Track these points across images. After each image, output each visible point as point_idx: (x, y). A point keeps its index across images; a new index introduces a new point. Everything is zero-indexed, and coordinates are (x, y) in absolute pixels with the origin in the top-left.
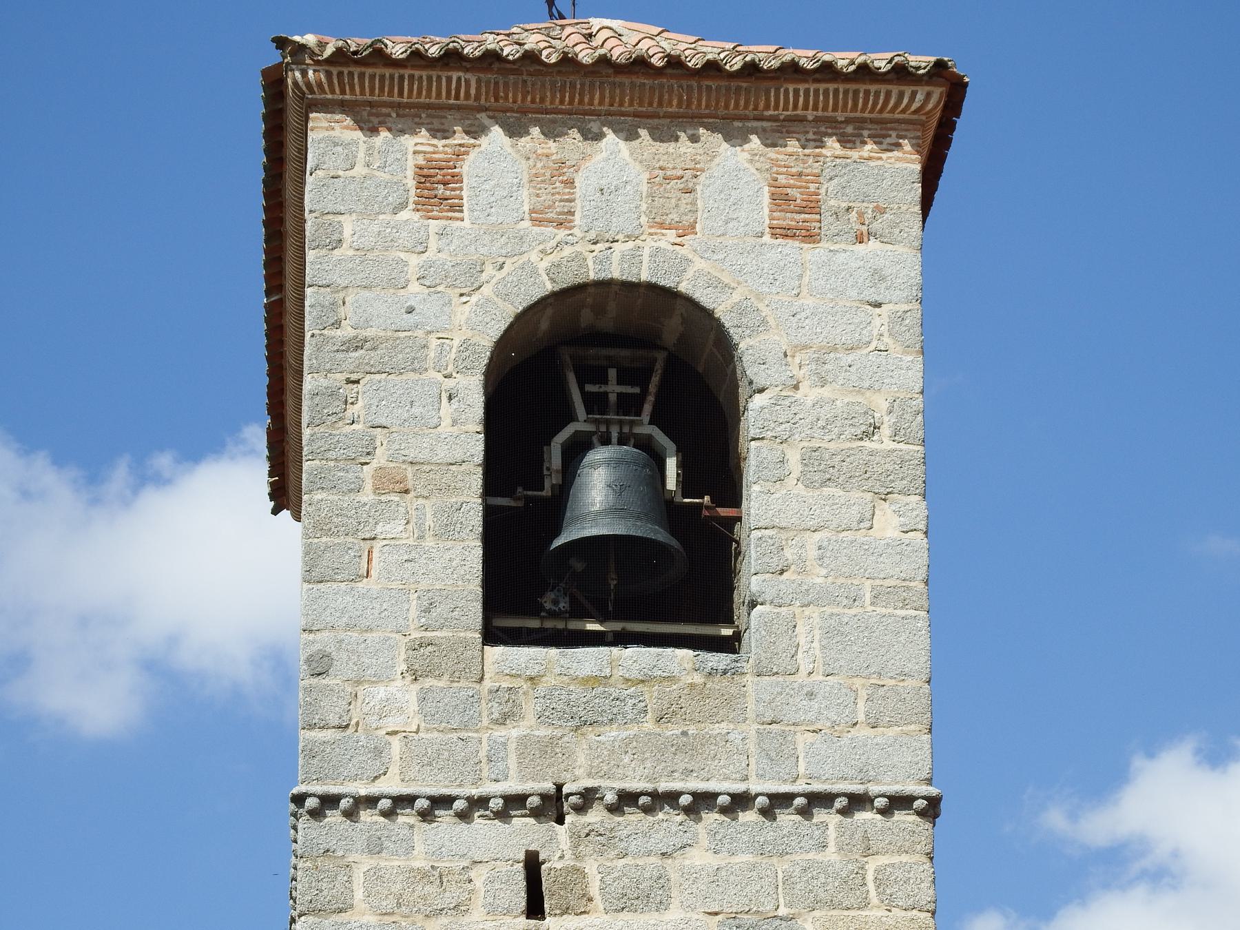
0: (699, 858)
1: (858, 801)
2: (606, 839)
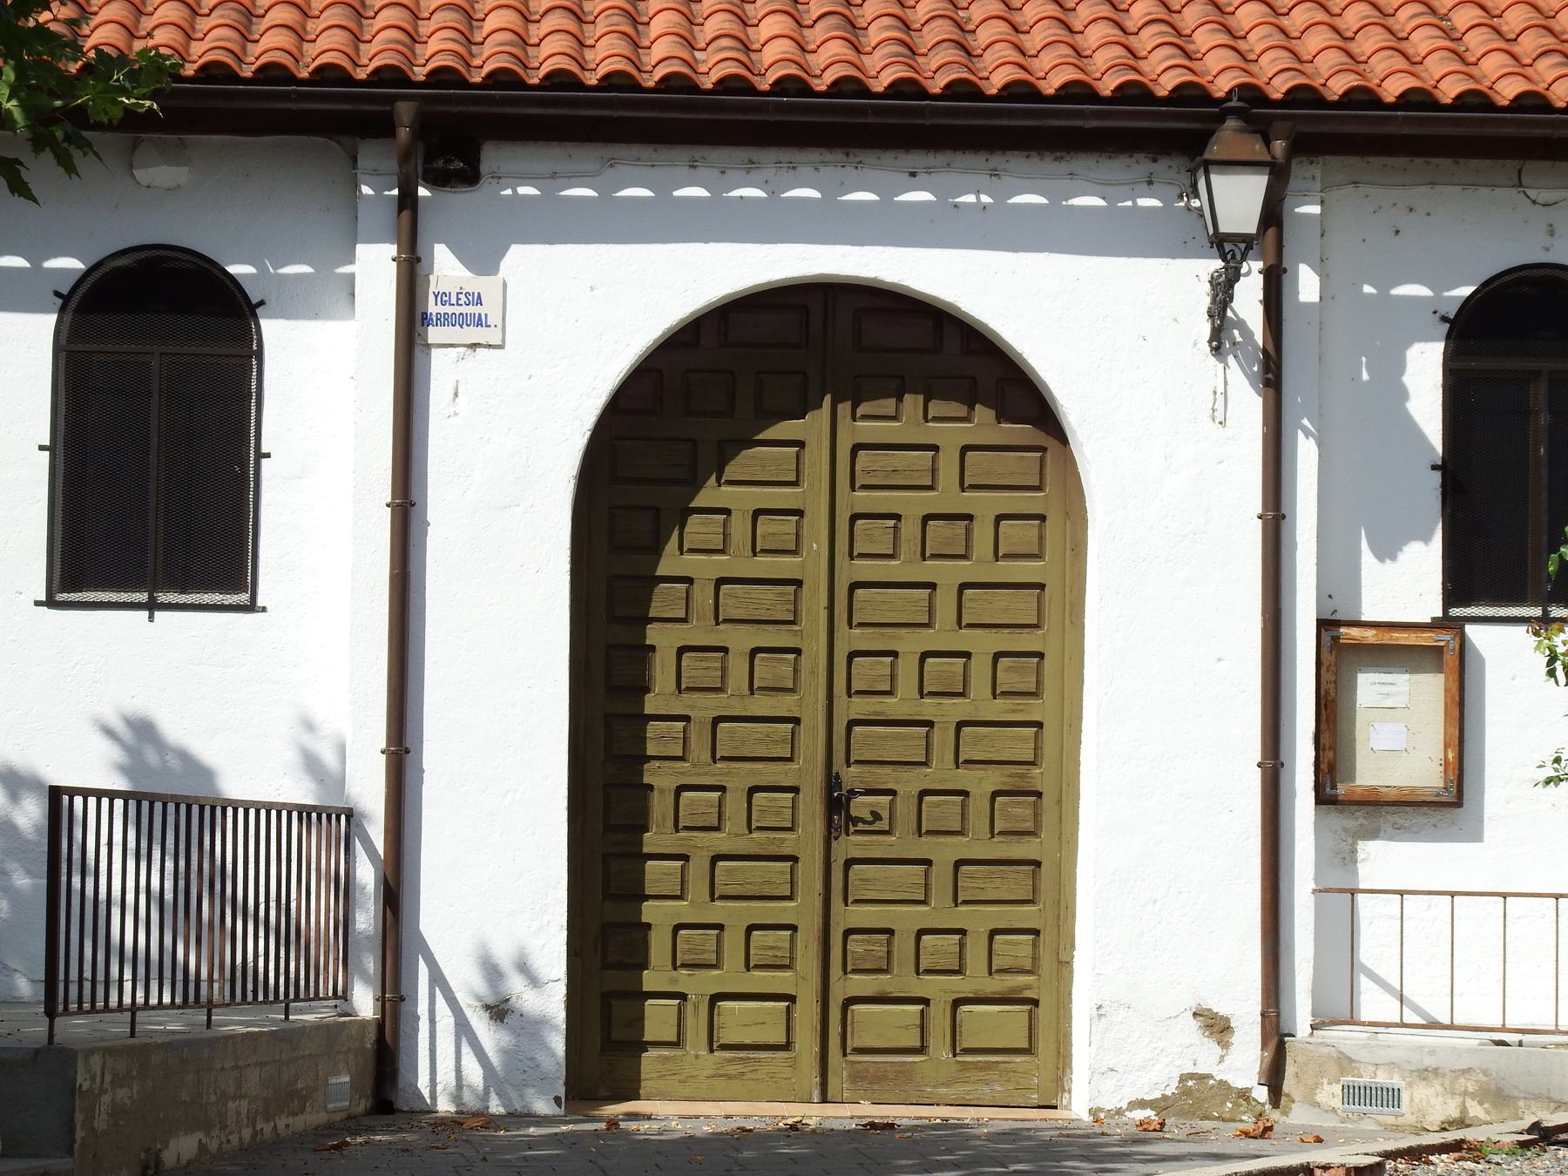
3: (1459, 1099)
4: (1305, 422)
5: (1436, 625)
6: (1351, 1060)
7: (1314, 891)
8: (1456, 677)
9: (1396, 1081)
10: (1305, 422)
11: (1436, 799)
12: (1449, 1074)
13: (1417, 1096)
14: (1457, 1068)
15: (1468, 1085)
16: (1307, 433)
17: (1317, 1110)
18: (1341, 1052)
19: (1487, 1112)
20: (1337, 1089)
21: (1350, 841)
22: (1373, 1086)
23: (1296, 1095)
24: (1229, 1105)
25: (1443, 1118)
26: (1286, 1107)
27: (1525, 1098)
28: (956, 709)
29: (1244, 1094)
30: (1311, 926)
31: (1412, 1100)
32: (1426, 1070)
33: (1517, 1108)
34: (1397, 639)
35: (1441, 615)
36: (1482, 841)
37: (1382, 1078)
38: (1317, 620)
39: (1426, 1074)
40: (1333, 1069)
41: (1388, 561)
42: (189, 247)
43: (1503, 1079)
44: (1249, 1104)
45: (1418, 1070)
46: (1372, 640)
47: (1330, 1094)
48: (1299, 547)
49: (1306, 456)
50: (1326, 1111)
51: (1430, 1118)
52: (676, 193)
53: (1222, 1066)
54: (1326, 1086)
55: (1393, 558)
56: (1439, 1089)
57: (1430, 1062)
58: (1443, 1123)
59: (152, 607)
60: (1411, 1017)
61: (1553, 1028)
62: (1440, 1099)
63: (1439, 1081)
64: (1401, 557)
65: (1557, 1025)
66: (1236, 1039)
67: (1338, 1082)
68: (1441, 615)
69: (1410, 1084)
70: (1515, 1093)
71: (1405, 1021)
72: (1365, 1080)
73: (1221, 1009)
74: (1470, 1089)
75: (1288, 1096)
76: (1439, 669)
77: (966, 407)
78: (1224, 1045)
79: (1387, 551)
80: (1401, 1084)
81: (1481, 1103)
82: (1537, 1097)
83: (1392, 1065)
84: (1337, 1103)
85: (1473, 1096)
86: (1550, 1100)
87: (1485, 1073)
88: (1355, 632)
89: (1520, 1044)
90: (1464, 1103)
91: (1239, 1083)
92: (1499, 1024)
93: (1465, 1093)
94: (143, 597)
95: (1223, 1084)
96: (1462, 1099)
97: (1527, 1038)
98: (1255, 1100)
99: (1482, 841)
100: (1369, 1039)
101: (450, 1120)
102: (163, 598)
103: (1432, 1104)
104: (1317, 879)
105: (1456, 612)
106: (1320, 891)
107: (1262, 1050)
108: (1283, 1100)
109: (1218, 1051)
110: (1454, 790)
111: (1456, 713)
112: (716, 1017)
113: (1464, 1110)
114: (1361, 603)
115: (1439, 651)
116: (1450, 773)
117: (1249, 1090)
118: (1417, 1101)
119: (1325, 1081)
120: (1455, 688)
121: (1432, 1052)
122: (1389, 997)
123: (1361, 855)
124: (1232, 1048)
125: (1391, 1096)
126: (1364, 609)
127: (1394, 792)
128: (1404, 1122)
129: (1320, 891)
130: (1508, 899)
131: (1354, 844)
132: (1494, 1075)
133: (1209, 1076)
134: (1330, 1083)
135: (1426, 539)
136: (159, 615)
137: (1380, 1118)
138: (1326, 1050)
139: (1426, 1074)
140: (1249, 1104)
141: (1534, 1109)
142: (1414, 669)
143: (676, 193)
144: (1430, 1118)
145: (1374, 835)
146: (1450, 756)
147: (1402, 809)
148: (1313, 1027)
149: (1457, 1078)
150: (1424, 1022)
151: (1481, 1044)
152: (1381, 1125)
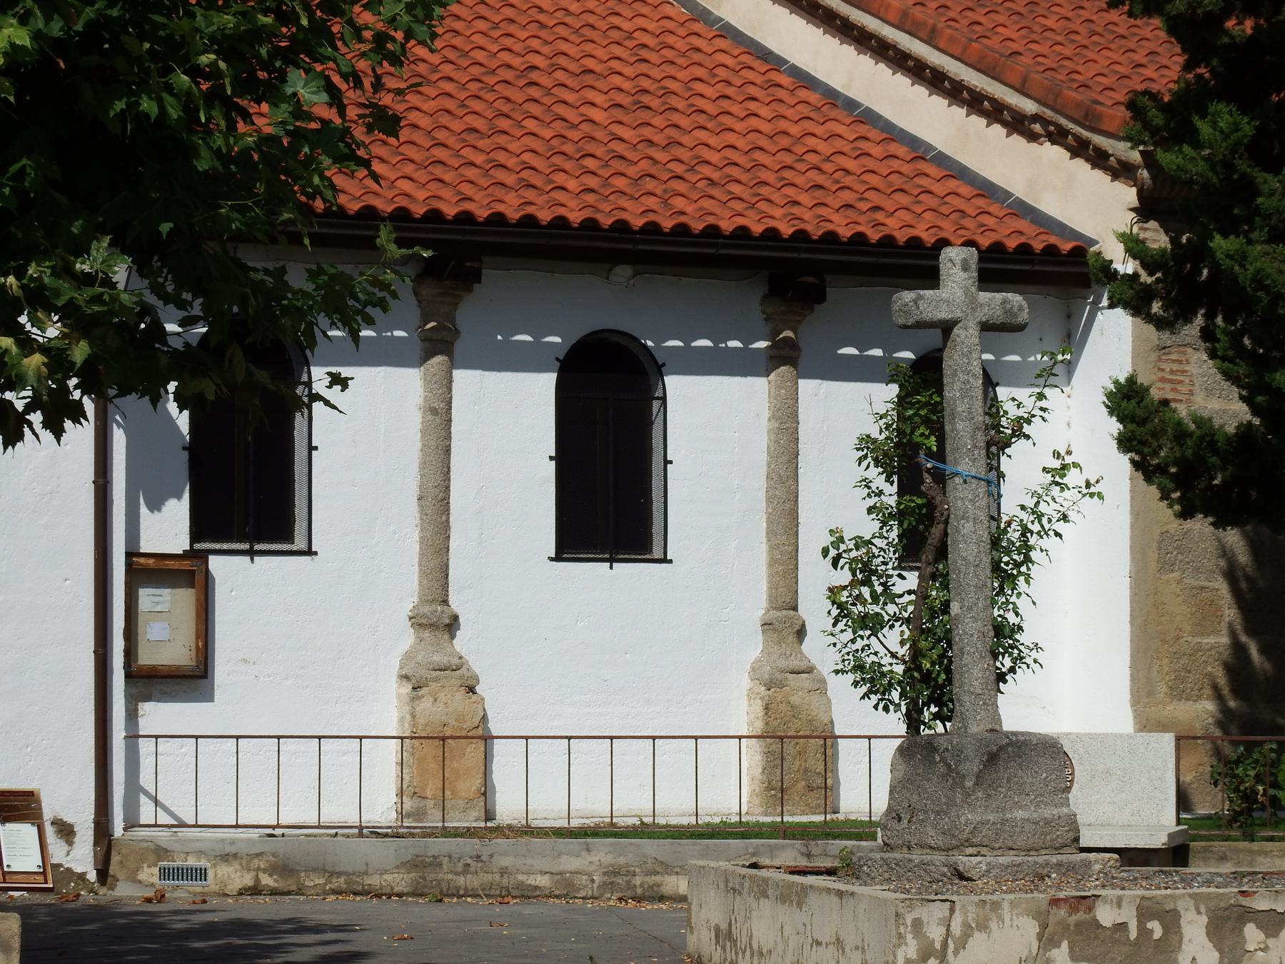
3: (253, 874)
4: (118, 417)
5: (185, 555)
6: (166, 851)
7: (126, 737)
8: (204, 591)
9: (203, 863)
10: (118, 417)
11: (192, 674)
12: (245, 857)
13: (220, 874)
14: (252, 853)
15: (261, 864)
16: (119, 425)
17: (139, 885)
18: (158, 846)
19: (275, 881)
20: (156, 871)
21: (134, 702)
22: (203, 867)
23: (120, 875)
24: (73, 884)
25: (240, 886)
26: (112, 884)
27: (305, 871)
29: (82, 876)
30: (123, 761)
31: (216, 876)
32: (228, 855)
33: (299, 877)
34: (168, 565)
35: (189, 549)
36: (213, 701)
37: (192, 862)
38: (126, 553)
39: (226, 858)
40: (152, 858)
41: (156, 512)
42: (566, 351)
43: (288, 859)
44: (84, 883)
45: (221, 856)
46: (153, 566)
47: (150, 874)
48: (115, 502)
49: (119, 439)
50: (146, 886)
51: (230, 887)
52: (839, 352)
53: (69, 858)
54: (146, 869)
55: (159, 510)
56: (238, 867)
57: (232, 849)
58: (240, 889)
59: (252, 553)
60: (164, 819)
61: (194, 823)
62: (238, 874)
63: (238, 862)
64: (164, 509)
65: (870, 817)
66: (77, 839)
67: (156, 865)
68: (189, 549)
69: (215, 865)
70: (298, 868)
71: (158, 823)
72: (179, 863)
73: (68, 818)
74: (262, 866)
75: (113, 876)
76: (193, 586)
77: (1160, 495)
78: (70, 843)
79: (155, 506)
80: (208, 865)
81: (271, 875)
82: (314, 870)
83: (200, 853)
84: (155, 880)
85: (264, 871)
86: (325, 871)
87: (274, 855)
88: (142, 560)
89: (283, 835)
90: (257, 875)
91: (79, 870)
92: (314, 821)
93: (258, 869)
94: (246, 546)
95: (69, 870)
96: (255, 873)
97: (340, 831)
98: (88, 880)
99: (213, 701)
100: (171, 836)
101: (45, 910)
102: (257, 547)
103: (233, 877)
104: (126, 730)
105: (197, 546)
106: (131, 737)
107: (94, 846)
108: (109, 880)
109: (66, 848)
110: (202, 667)
111: (203, 615)
112: (383, 825)
113: (257, 880)
114: (139, 540)
115: (192, 573)
116: (200, 655)
117: (85, 874)
118: (219, 876)
119: (145, 865)
120: (203, 598)
121: (232, 842)
122: (167, 804)
123: (141, 713)
124: (75, 845)
125: (201, 874)
126: (142, 544)
127: (167, 668)
128: (211, 890)
129: (131, 737)
130: (699, 740)
131: (137, 705)
132: (281, 856)
133: (61, 865)
134: (149, 867)
135: (179, 497)
136: (256, 559)
137: (189, 888)
138: (146, 845)
139: (226, 858)
140: (84, 883)
141: (312, 877)
142: (173, 586)
143: (839, 352)
144: (230, 887)
145: (148, 698)
146: (200, 644)
147: (165, 680)
148: (125, 830)
149: (252, 859)
150: (176, 823)
151: (260, 837)
152: (190, 893)
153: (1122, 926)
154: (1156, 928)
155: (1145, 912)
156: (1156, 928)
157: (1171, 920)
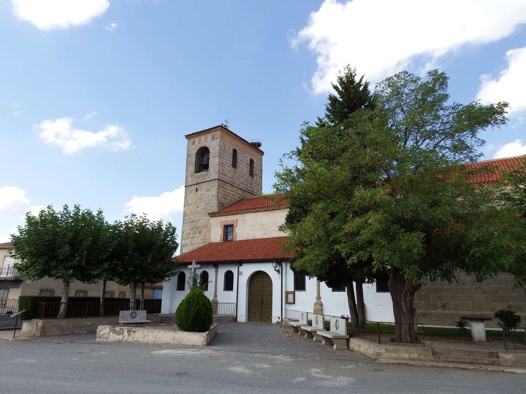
0: (205, 186)
1: (214, 180)
2: (200, 185)
28: (256, 297)
153: (118, 330)
154: (121, 331)
155: (120, 329)
156: (121, 331)
157: (123, 330)
